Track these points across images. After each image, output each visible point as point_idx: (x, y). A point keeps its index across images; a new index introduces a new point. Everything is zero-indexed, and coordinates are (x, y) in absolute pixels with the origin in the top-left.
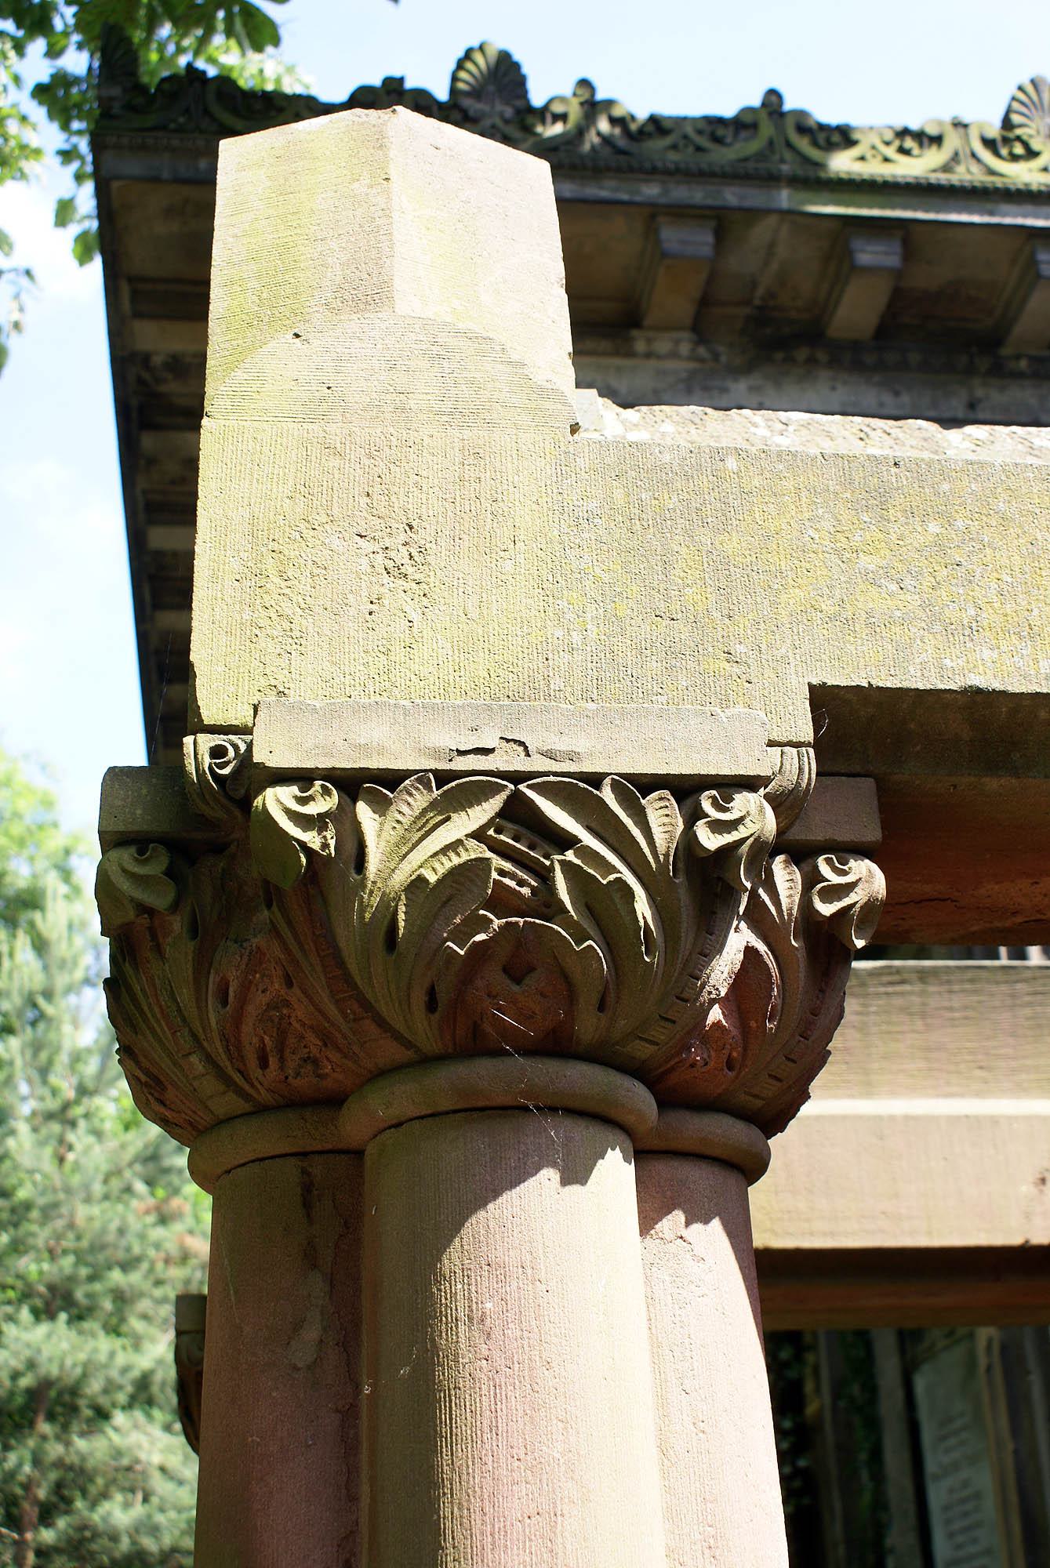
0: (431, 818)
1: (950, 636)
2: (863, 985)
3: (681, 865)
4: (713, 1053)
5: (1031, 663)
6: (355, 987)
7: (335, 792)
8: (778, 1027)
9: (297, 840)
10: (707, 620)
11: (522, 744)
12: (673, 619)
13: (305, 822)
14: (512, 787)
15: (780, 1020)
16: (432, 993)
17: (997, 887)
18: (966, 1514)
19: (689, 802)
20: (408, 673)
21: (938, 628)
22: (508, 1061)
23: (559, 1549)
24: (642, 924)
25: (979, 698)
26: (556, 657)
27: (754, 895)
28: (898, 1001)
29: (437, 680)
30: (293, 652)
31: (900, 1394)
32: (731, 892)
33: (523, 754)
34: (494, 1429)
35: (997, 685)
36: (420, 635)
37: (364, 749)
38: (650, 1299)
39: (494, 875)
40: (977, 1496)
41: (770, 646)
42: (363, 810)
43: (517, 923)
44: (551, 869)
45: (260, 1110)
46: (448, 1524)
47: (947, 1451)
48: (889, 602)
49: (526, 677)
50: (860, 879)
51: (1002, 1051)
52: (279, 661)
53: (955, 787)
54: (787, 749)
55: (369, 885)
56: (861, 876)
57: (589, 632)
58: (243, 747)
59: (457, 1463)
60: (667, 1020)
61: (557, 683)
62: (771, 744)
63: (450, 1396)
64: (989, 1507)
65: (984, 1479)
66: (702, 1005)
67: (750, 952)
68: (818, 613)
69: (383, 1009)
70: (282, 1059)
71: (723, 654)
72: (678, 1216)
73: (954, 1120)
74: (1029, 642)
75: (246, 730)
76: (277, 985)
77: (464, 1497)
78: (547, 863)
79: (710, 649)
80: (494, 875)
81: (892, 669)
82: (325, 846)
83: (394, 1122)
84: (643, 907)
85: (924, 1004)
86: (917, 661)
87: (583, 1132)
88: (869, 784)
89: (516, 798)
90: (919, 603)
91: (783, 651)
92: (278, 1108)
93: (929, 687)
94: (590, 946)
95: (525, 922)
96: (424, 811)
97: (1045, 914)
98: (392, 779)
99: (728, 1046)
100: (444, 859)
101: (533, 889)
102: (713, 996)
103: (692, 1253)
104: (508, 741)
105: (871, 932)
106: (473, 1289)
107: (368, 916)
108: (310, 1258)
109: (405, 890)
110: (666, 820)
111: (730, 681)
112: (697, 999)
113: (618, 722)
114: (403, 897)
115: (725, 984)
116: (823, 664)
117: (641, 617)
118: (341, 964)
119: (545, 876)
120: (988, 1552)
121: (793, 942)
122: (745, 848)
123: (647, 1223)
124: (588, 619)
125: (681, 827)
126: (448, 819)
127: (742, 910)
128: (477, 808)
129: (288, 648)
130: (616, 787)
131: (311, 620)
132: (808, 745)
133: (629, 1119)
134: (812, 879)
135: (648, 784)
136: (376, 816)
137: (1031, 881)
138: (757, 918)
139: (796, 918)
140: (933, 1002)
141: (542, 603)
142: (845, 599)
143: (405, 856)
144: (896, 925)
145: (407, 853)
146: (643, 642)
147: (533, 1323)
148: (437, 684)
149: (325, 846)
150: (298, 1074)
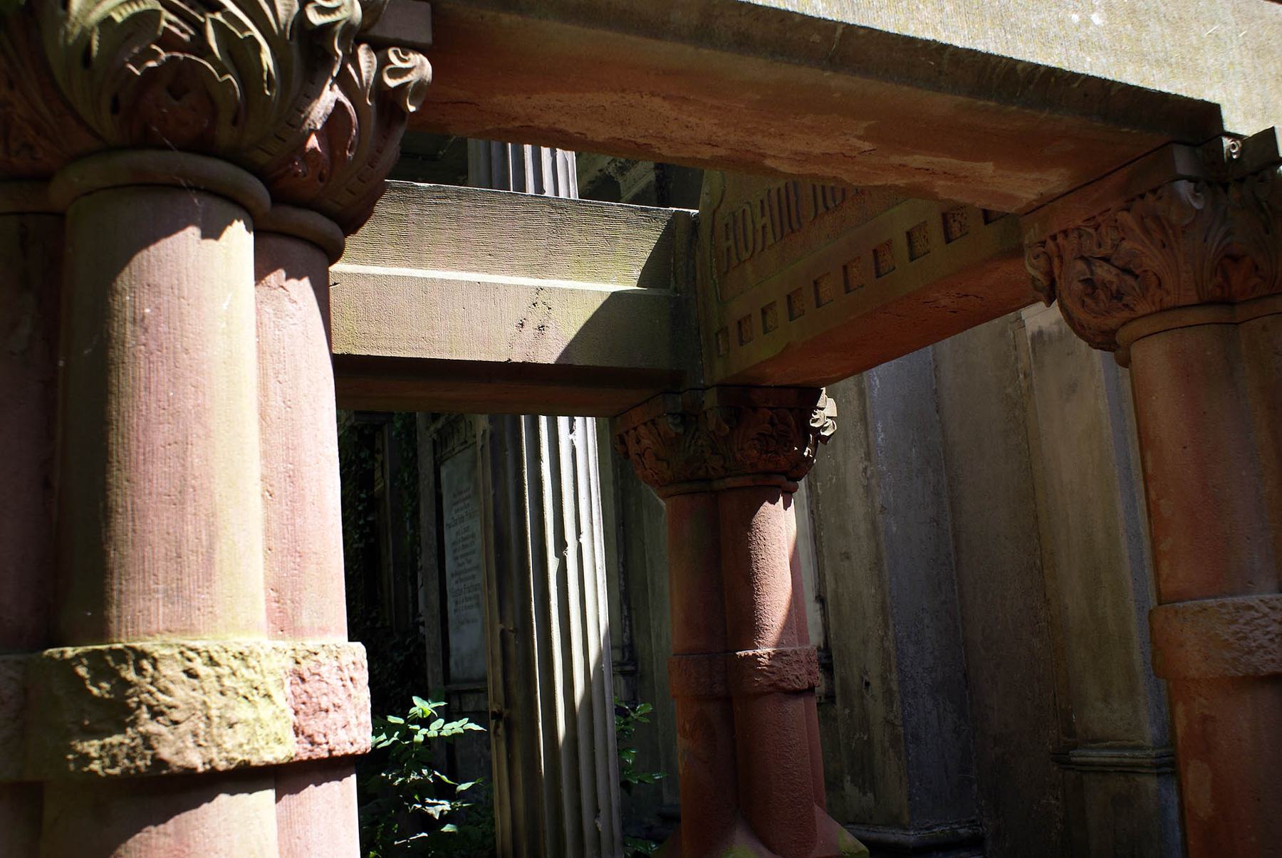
3: (295, 33)
8: (354, 157)
17: (504, 98)
18: (465, 546)
23: (189, 465)
24: (265, 67)
31: (432, 478)
32: (329, 58)
34: (147, 388)
38: (259, 325)
39: (164, 23)
40: (473, 536)
43: (177, 57)
44: (205, 24)
46: (114, 447)
47: (457, 511)
53: (482, 17)
55: (72, 19)
59: (122, 410)
60: (280, 138)
64: (479, 542)
65: (476, 526)
67: (338, 103)
72: (282, 273)
77: (126, 430)
78: (202, 20)
80: (164, 23)
84: (267, 58)
87: (218, 206)
88: (427, 6)
95: (185, 58)
97: (533, 122)
102: (312, 127)
105: (420, 102)
106: (137, 300)
112: (300, 128)
114: (97, 30)
115: (321, 121)
119: (200, 29)
120: (477, 567)
121: (369, 102)
122: (339, 27)
123: (260, 275)
125: (296, 8)
127: (335, 74)
134: (384, 62)
138: (344, 82)
140: (464, 212)
147: (178, 324)
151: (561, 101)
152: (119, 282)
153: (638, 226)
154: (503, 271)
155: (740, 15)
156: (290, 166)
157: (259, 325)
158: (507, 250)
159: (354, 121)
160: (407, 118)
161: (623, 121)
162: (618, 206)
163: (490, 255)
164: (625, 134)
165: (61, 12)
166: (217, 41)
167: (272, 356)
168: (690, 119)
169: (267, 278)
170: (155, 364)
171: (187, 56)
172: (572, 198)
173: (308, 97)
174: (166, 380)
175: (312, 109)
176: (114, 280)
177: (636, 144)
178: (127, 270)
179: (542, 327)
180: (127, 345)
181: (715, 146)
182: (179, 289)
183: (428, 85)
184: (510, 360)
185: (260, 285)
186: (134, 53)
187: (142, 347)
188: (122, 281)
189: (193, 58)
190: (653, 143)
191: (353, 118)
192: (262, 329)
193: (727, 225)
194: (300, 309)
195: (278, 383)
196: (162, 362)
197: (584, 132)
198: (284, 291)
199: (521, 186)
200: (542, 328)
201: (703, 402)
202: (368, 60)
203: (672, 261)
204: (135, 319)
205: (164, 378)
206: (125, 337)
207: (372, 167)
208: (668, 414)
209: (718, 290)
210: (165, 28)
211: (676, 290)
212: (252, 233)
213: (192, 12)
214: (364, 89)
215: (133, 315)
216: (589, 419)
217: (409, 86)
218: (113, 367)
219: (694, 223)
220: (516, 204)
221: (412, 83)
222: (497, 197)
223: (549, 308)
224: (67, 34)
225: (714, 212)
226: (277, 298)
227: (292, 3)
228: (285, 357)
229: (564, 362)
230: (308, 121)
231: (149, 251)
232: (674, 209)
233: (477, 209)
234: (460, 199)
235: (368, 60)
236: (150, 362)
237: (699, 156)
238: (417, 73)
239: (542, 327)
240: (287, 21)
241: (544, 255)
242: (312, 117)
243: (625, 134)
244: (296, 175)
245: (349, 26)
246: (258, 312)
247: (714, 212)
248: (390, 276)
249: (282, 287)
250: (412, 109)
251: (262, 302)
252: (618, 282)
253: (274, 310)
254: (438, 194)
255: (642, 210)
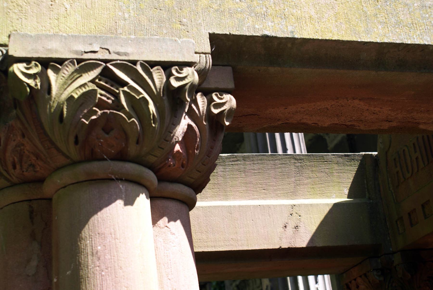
0: (75, 75)
1: (257, 18)
2: (224, 162)
3: (165, 93)
4: (177, 162)
5: (285, 27)
6: (47, 136)
7: (40, 66)
8: (199, 153)
9: (26, 83)
10: (173, 10)
11: (107, 49)
12: (161, 10)
13: (28, 76)
14: (104, 64)
15: (200, 149)
16: (76, 137)
17: (273, 110)
19: (168, 71)
20: (66, 27)
21: (253, 14)
22: (105, 162)
24: (152, 113)
25: (267, 39)
26: (119, 22)
27: (190, 107)
28: (236, 167)
29: (76, 29)
30: (23, 19)
32: (183, 103)
33: (108, 53)
35: (274, 35)
36: (70, 13)
37: (50, 50)
38: (156, 248)
41: (195, 19)
42: (50, 73)
43: (107, 112)
44: (119, 93)
45: (13, 185)
48: (236, 6)
49: (108, 28)
50: (227, 101)
51: (271, 184)
52: (17, 22)
54: (201, 55)
55: (53, 99)
56: (227, 100)
57: (131, 14)
58: (5, 52)
60: (161, 148)
61: (119, 31)
62: (196, 53)
63: (86, 280)
66: (173, 143)
67: (189, 126)
68: (212, 9)
69: (59, 144)
70: (21, 166)
71: (178, 22)
72: (165, 219)
73: (255, 207)
74: (284, 20)
75: (5, 46)
76: (19, 138)
78: (117, 91)
79: (174, 20)
80: (99, 96)
81: (238, 28)
82: (36, 85)
83: (63, 186)
84: (152, 108)
85: (244, 168)
86: (246, 26)
87: (131, 187)
88: (229, 69)
89: (106, 69)
90: (246, 6)
91: (200, 21)
92: (20, 184)
93: (250, 34)
94: (133, 121)
95: (110, 112)
96: (73, 73)
98: (61, 61)
99: (182, 159)
100: (80, 90)
101: (113, 101)
102: (177, 140)
103: (170, 232)
104: (103, 48)
105: (231, 120)
106: (93, 242)
107: (52, 110)
108: (33, 236)
109: (66, 101)
110: (160, 77)
111: (181, 32)
112: (171, 141)
113: (142, 43)
114: (66, 103)
116: (214, 26)
117: (149, 9)
118: (43, 128)
119: (117, 96)
122: (188, 87)
123: (155, 221)
124: (131, 9)
125: (165, 80)
126: (81, 76)
127: (186, 110)
128: (92, 72)
129: (21, 17)
130: (142, 65)
131: (29, 7)
132: (209, 53)
133: (148, 184)
134: (210, 101)
135: (153, 64)
136: (55, 75)
137: (285, 108)
138: (191, 114)
139: (205, 114)
140: (248, 167)
141: (114, 3)
142: (221, 4)
143: (66, 89)
144: (238, 125)
145: (67, 88)
146: (150, 18)
147: (115, 253)
148: (76, 31)
149: (36, 85)
150: (27, 171)
151: (303, 108)
152: (83, 233)
153: (344, 165)
154: (272, 198)
155: (399, 51)
156: (167, 162)
157: (156, 248)
158: (273, 186)
159: (198, 134)
160: (225, 129)
161: (338, 114)
162: (332, 155)
163: (264, 189)
164: (340, 121)
165: (47, 96)
166: (126, 101)
167: (164, 265)
168: (375, 109)
169: (158, 223)
170: (105, 277)
171: (111, 111)
172: (303, 153)
173: (174, 125)
174: (111, 285)
175: (176, 131)
176: (80, 232)
177: (346, 125)
178: (87, 226)
179: (297, 226)
180: (89, 267)
181: (391, 121)
182: (115, 234)
183: (234, 110)
184: (281, 247)
185: (155, 226)
186: (85, 113)
187: (98, 268)
188: (85, 233)
189: (115, 112)
190: (355, 124)
191: (197, 133)
192: (158, 250)
193: (395, 159)
194: (177, 238)
195: (168, 280)
196: (108, 275)
197: (317, 122)
198: (168, 229)
199: (274, 150)
200: (296, 227)
201: (393, 261)
202: (202, 100)
203: (365, 182)
204: (92, 253)
205: (110, 284)
206: (88, 263)
207: (209, 157)
208: (374, 270)
209: (394, 197)
210: (99, 98)
211: (370, 199)
212: (149, 199)
213: (112, 88)
214: (201, 117)
215: (91, 251)
216: (326, 276)
217: (225, 112)
218: (83, 280)
219: (375, 159)
220: (276, 160)
221: (227, 110)
222: (265, 157)
223: (300, 216)
224: (51, 107)
225: (386, 153)
226: (164, 233)
227: (162, 77)
228: (171, 265)
229: (311, 246)
230: (175, 137)
231: (98, 215)
232: (364, 153)
233: (255, 165)
234: (245, 161)
235: (202, 100)
236: (102, 276)
237: (382, 128)
238: (228, 105)
239: (297, 226)
240: (161, 86)
241: (293, 187)
242: (176, 135)
243: (340, 121)
244: (170, 166)
245: (192, 86)
246: (155, 241)
247: (386, 153)
248: (211, 206)
249: (166, 226)
250: (227, 123)
251: (156, 236)
252: (337, 197)
253: (163, 240)
254: (233, 159)
255: (345, 156)
